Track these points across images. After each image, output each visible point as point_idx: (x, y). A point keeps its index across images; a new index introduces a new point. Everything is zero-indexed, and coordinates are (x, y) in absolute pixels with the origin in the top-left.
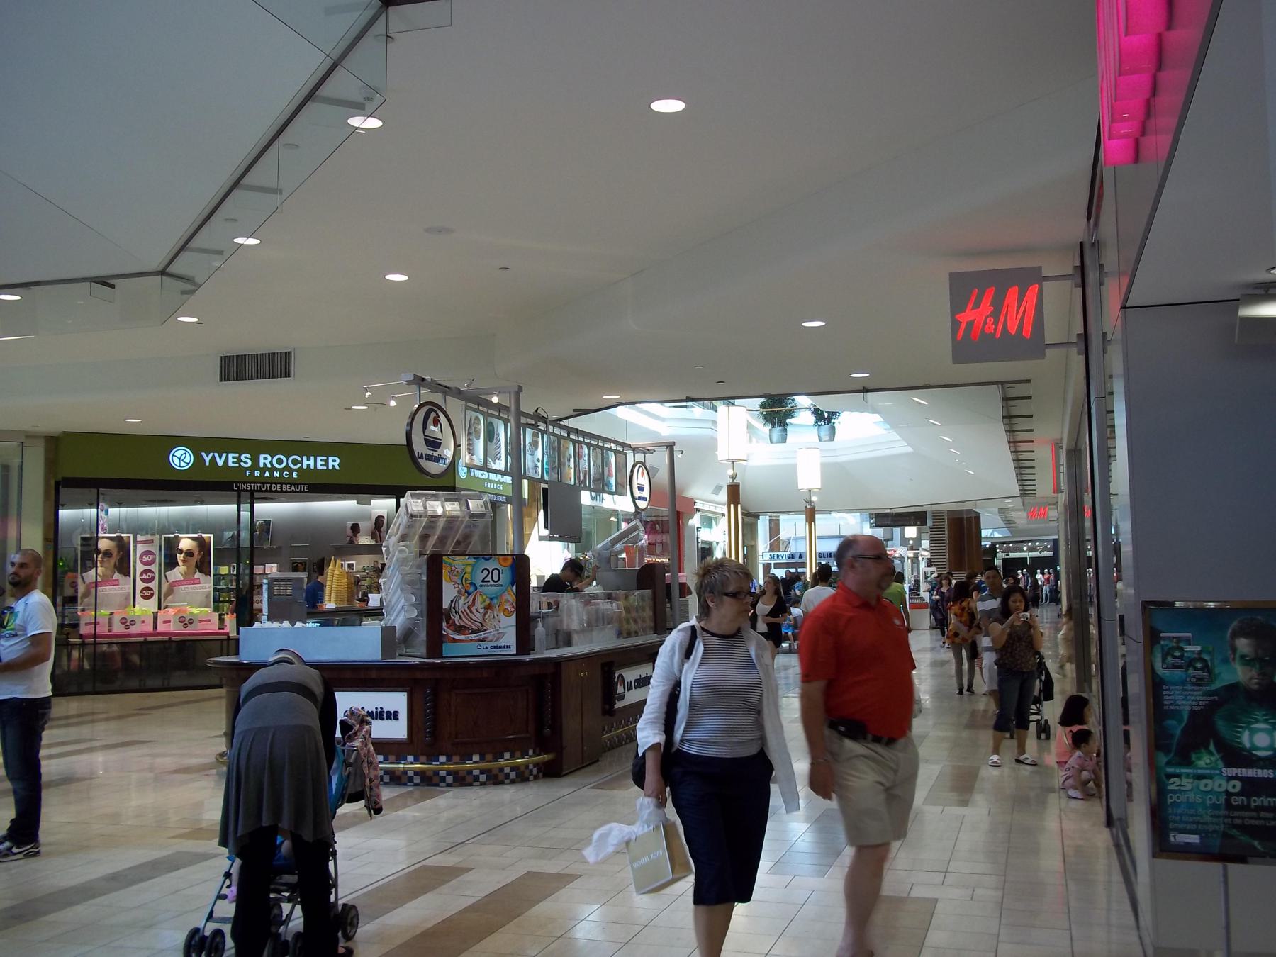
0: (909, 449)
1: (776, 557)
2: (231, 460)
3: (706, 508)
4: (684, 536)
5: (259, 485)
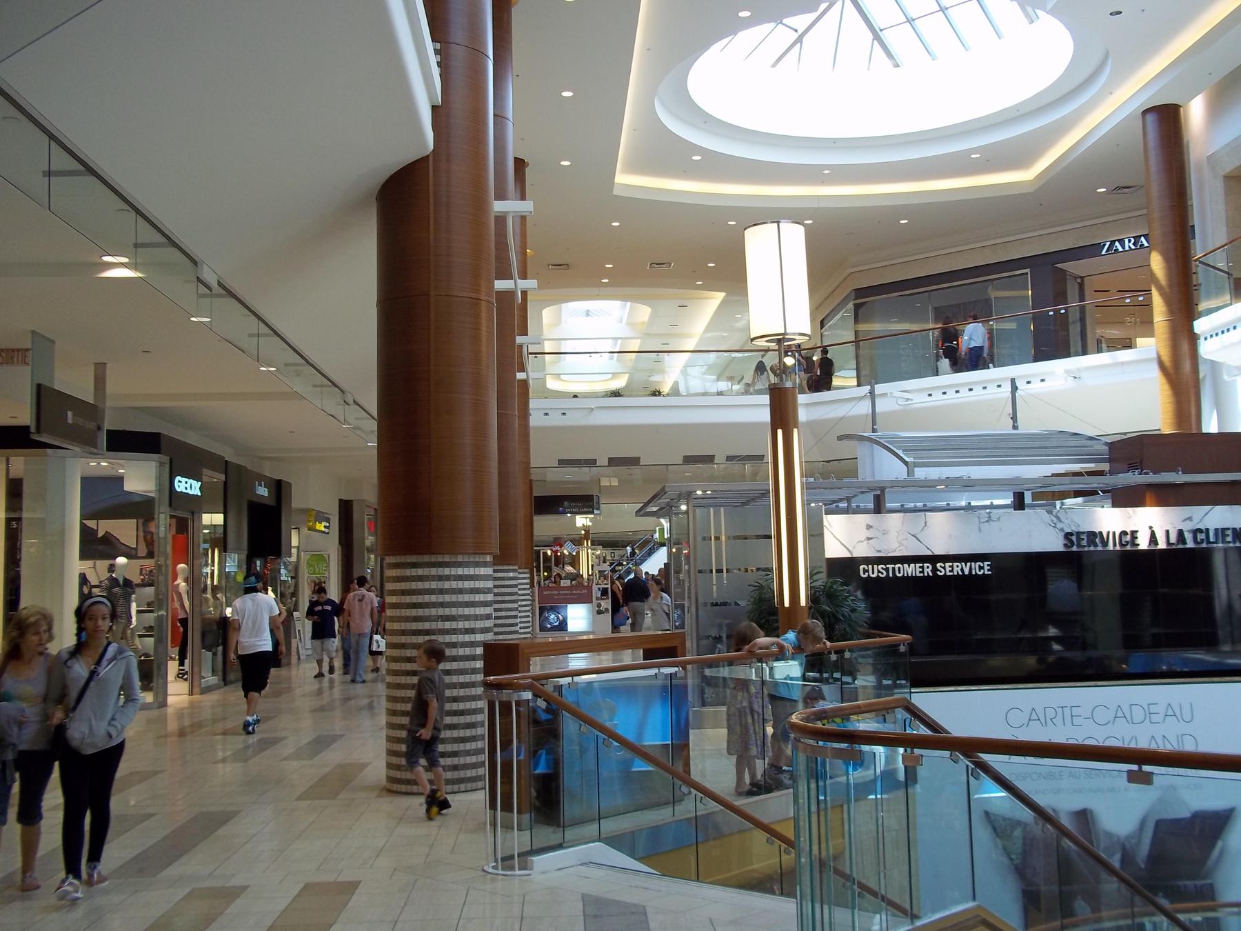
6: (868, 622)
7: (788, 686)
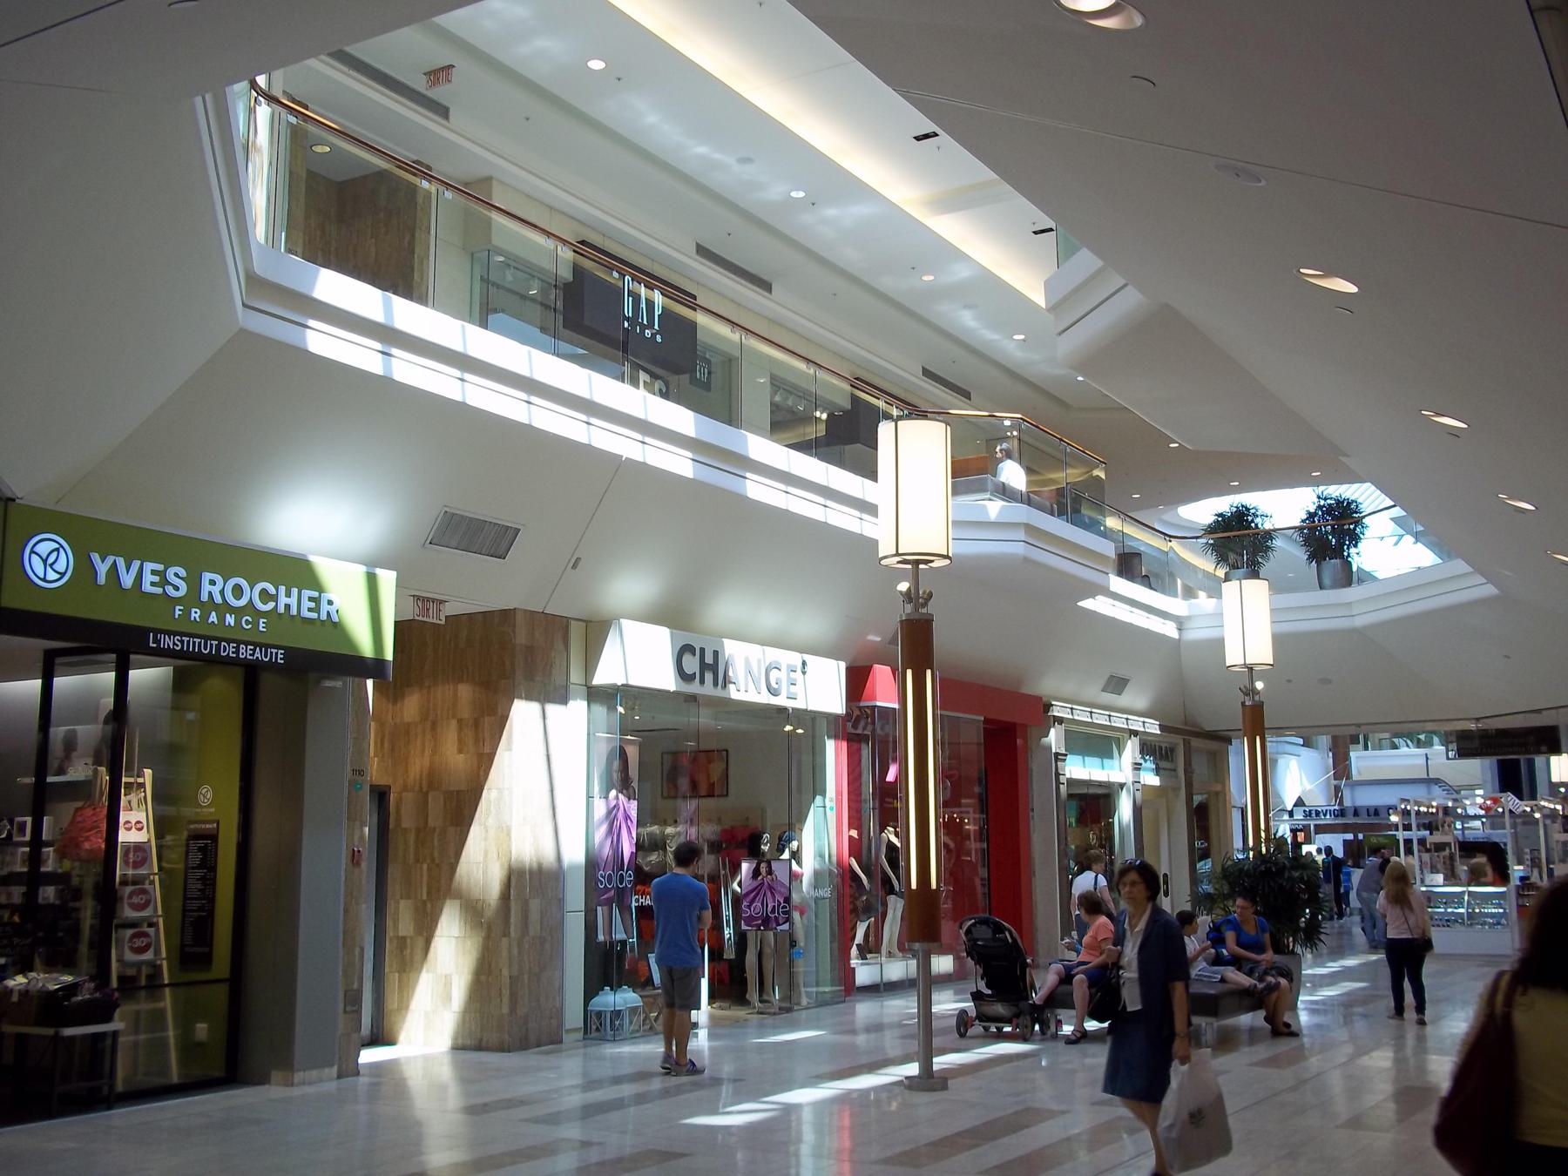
0: (1490, 590)
1: (1314, 815)
2: (148, 578)
3: (1082, 715)
4: (1028, 771)
5: (197, 640)
6: (1208, 906)
7: (1089, 472)
